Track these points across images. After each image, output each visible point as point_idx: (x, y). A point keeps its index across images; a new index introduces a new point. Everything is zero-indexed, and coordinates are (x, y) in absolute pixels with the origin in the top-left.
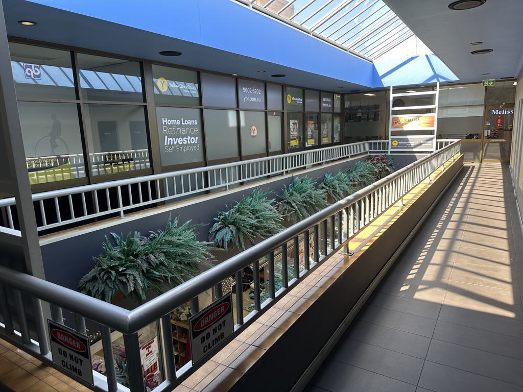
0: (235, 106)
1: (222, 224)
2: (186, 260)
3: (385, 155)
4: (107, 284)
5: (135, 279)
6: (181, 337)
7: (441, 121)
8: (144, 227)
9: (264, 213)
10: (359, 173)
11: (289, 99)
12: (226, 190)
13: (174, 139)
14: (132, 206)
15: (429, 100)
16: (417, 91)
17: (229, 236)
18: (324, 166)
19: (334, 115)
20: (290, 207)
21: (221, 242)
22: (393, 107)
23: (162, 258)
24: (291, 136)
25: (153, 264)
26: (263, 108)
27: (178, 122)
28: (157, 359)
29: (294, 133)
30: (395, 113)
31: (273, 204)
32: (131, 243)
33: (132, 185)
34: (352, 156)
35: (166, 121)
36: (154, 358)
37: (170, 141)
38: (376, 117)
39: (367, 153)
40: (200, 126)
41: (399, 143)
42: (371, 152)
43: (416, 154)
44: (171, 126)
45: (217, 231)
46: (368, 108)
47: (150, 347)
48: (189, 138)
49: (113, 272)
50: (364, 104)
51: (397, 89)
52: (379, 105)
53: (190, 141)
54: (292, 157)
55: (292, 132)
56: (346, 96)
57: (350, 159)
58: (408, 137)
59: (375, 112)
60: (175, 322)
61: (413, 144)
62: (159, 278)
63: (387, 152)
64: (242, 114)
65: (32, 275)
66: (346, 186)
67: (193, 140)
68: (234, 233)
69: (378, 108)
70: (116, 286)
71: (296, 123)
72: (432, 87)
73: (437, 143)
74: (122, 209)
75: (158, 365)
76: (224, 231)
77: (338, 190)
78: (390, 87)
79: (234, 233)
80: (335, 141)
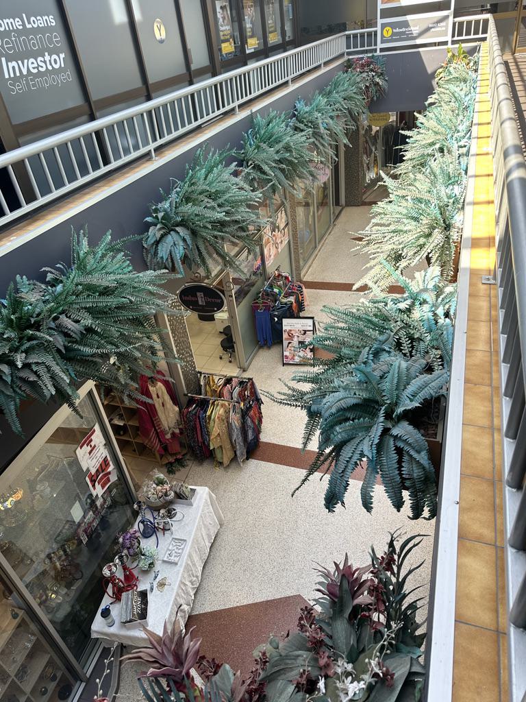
2: (131, 315)
5: (48, 368)
10: (342, 94)
12: (150, 159)
13: (20, 62)
17: (181, 248)
21: (170, 260)
23: (88, 321)
24: (221, 33)
25: (74, 335)
27: (17, 23)
28: (107, 452)
29: (225, 28)
31: (236, 174)
33: (353, 35)
34: (326, 64)
36: (102, 452)
37: (13, 68)
39: (342, 55)
41: (394, 30)
42: (349, 54)
45: (157, 243)
47: (91, 440)
48: (47, 58)
53: (51, 64)
54: (231, 80)
57: (323, 70)
58: (409, 18)
61: (415, 30)
68: (189, 242)
70: (17, 389)
71: (225, 6)
73: (454, 24)
75: (109, 459)
76: (169, 239)
77: (322, 130)
79: (189, 242)
80: (287, 39)
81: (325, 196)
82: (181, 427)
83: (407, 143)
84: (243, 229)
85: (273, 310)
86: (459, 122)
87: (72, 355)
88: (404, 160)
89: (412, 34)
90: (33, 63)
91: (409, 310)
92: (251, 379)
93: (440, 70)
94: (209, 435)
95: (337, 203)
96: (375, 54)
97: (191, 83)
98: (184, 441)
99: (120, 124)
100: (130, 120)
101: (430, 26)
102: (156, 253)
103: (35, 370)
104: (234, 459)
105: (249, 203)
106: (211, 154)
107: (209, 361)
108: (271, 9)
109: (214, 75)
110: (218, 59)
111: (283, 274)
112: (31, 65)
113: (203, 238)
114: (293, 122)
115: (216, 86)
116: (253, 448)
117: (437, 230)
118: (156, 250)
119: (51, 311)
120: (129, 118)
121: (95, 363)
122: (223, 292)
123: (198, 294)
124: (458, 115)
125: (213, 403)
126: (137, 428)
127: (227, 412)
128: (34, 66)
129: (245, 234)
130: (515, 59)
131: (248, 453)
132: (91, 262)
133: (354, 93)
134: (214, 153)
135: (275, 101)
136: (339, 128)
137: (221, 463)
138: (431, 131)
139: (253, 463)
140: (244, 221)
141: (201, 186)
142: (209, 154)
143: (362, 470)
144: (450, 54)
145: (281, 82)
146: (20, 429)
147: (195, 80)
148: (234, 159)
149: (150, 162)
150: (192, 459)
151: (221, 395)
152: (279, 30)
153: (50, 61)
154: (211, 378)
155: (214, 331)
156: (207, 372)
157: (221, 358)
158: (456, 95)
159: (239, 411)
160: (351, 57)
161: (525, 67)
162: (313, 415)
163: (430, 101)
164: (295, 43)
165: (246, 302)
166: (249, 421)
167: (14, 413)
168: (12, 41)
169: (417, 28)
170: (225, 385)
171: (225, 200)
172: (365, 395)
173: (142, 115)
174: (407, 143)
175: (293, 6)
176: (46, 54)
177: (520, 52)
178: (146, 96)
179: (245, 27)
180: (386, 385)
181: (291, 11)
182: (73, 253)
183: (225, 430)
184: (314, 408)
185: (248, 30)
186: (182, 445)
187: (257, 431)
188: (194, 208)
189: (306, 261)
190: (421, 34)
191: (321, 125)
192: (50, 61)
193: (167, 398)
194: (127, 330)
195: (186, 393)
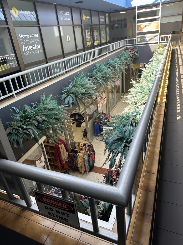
0: (56, 24)
1: (67, 94)
2: (56, 117)
3: (134, 47)
4: (18, 135)
6: (51, 150)
7: (162, 25)
8: (29, 101)
9: (86, 86)
10: (124, 58)
11: (84, 17)
13: (28, 47)
14: (19, 90)
15: (154, 13)
16: (147, 9)
17: (72, 100)
18: (108, 55)
19: (106, 25)
20: (96, 80)
21: (68, 104)
22: (137, 19)
23: (44, 118)
24: (87, 39)
26: (71, 24)
27: (28, 36)
29: (88, 38)
30: (139, 22)
31: (89, 80)
32: (25, 111)
34: (119, 49)
35: (21, 36)
37: (26, 48)
38: (125, 26)
39: (125, 46)
40: (40, 38)
41: (141, 39)
42: (127, 46)
43: (149, 45)
44: (25, 39)
45: (65, 98)
46: (121, 20)
47: (41, 159)
48: (35, 46)
49: (20, 129)
50: (119, 18)
51: (140, 8)
52: (127, 19)
53: (36, 47)
54: (89, 53)
55: (87, 37)
56: (111, 14)
58: (146, 35)
59: (125, 23)
60: (47, 144)
61: (147, 39)
62: (44, 128)
63: (135, 45)
64: (61, 27)
65: (7, 159)
66: (120, 66)
67: (38, 47)
68: (74, 98)
69: (126, 20)
71: (88, 32)
72: (157, 5)
73: (160, 37)
74: (14, 93)
76: (68, 98)
77: (117, 68)
78: (135, 7)
79: (74, 98)
80: (108, 41)
81: (119, 89)
82: (68, 159)
83: (142, 72)
84: (90, 96)
85: (100, 124)
86: (158, 66)
87: (39, 127)
88: (141, 77)
89: (147, 40)
90: (31, 47)
91: (136, 116)
92: (92, 144)
93: (156, 51)
94: (77, 162)
95: (123, 92)
96: (135, 46)
97: (77, 53)
98: (69, 165)
99: (56, 64)
100: (59, 63)
101: (152, 38)
102: (64, 102)
103: (28, 130)
104: (85, 171)
105: (93, 88)
106: (82, 74)
107: (78, 138)
108: (103, 32)
109: (84, 51)
110: (86, 47)
111: (104, 113)
112: (31, 47)
113: (79, 99)
114: (108, 66)
115: (84, 54)
116: (92, 168)
117: (147, 96)
118: (64, 100)
119: (34, 115)
120: (50, 66)
121: (45, 130)
122: (84, 115)
123: (76, 116)
124: (158, 64)
125: (79, 152)
126: (54, 159)
127: (84, 155)
128: (31, 48)
129: (91, 97)
130: (180, 48)
131: (90, 169)
132: (46, 102)
133: (128, 57)
134: (83, 74)
135: (102, 60)
136: (123, 68)
137: (81, 173)
138: (149, 69)
139: (92, 173)
140: (91, 93)
141: (79, 83)
142: (81, 74)
143: (120, 155)
144: (159, 46)
145: (104, 54)
146: (23, 147)
147: (78, 53)
148: (89, 76)
149: (64, 76)
150: (72, 171)
151: (82, 149)
152: (105, 39)
153: (36, 46)
154: (79, 144)
155: (81, 131)
156: (77, 142)
157: (83, 139)
158: (159, 58)
159: (88, 154)
160: (127, 47)
161: (182, 51)
162: (107, 143)
163: (151, 60)
164: (110, 42)
165: (91, 121)
166: (91, 158)
167: (22, 142)
168: (26, 41)
169: (148, 38)
170: (83, 146)
171: (85, 87)
172: (120, 136)
173: (62, 62)
174: (142, 72)
175: (110, 32)
176: (35, 45)
177: (182, 46)
178: (46, 62)
179: (95, 38)
180: (127, 133)
181: (109, 33)
182: (41, 99)
183: (83, 161)
184: (107, 141)
185: (95, 38)
186: (69, 166)
187: (93, 162)
188: (76, 89)
189: (112, 109)
190: (149, 40)
191: (116, 67)
192: (36, 46)
193: (65, 149)
194: (54, 121)
195: (71, 148)
